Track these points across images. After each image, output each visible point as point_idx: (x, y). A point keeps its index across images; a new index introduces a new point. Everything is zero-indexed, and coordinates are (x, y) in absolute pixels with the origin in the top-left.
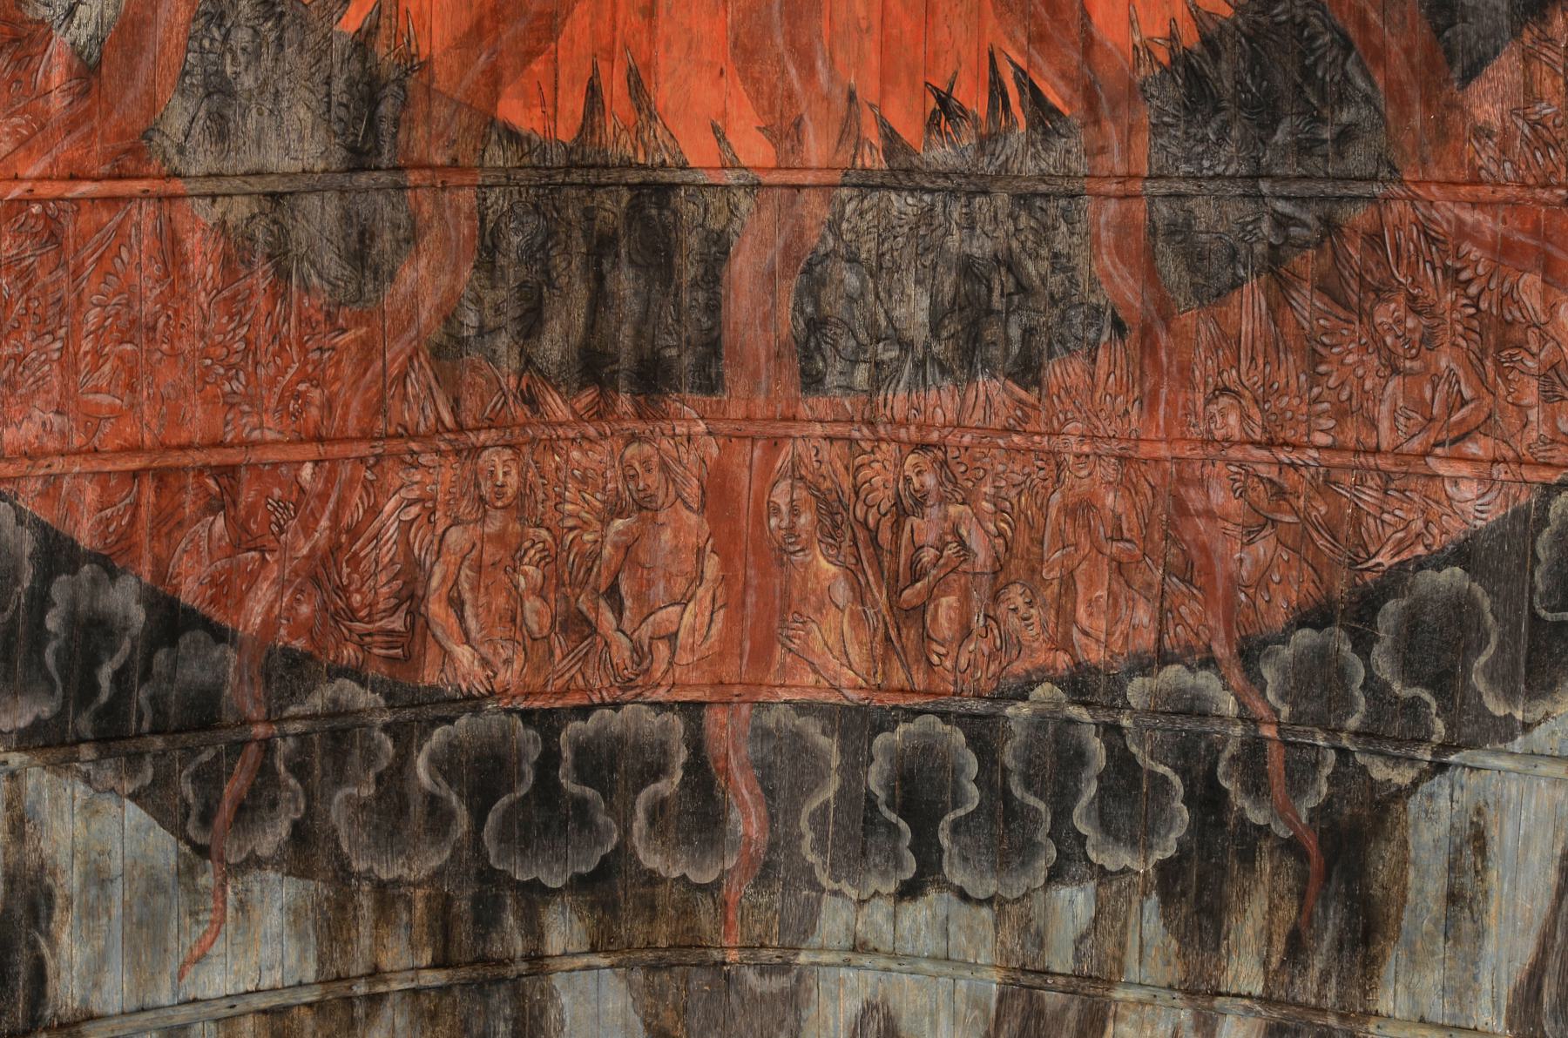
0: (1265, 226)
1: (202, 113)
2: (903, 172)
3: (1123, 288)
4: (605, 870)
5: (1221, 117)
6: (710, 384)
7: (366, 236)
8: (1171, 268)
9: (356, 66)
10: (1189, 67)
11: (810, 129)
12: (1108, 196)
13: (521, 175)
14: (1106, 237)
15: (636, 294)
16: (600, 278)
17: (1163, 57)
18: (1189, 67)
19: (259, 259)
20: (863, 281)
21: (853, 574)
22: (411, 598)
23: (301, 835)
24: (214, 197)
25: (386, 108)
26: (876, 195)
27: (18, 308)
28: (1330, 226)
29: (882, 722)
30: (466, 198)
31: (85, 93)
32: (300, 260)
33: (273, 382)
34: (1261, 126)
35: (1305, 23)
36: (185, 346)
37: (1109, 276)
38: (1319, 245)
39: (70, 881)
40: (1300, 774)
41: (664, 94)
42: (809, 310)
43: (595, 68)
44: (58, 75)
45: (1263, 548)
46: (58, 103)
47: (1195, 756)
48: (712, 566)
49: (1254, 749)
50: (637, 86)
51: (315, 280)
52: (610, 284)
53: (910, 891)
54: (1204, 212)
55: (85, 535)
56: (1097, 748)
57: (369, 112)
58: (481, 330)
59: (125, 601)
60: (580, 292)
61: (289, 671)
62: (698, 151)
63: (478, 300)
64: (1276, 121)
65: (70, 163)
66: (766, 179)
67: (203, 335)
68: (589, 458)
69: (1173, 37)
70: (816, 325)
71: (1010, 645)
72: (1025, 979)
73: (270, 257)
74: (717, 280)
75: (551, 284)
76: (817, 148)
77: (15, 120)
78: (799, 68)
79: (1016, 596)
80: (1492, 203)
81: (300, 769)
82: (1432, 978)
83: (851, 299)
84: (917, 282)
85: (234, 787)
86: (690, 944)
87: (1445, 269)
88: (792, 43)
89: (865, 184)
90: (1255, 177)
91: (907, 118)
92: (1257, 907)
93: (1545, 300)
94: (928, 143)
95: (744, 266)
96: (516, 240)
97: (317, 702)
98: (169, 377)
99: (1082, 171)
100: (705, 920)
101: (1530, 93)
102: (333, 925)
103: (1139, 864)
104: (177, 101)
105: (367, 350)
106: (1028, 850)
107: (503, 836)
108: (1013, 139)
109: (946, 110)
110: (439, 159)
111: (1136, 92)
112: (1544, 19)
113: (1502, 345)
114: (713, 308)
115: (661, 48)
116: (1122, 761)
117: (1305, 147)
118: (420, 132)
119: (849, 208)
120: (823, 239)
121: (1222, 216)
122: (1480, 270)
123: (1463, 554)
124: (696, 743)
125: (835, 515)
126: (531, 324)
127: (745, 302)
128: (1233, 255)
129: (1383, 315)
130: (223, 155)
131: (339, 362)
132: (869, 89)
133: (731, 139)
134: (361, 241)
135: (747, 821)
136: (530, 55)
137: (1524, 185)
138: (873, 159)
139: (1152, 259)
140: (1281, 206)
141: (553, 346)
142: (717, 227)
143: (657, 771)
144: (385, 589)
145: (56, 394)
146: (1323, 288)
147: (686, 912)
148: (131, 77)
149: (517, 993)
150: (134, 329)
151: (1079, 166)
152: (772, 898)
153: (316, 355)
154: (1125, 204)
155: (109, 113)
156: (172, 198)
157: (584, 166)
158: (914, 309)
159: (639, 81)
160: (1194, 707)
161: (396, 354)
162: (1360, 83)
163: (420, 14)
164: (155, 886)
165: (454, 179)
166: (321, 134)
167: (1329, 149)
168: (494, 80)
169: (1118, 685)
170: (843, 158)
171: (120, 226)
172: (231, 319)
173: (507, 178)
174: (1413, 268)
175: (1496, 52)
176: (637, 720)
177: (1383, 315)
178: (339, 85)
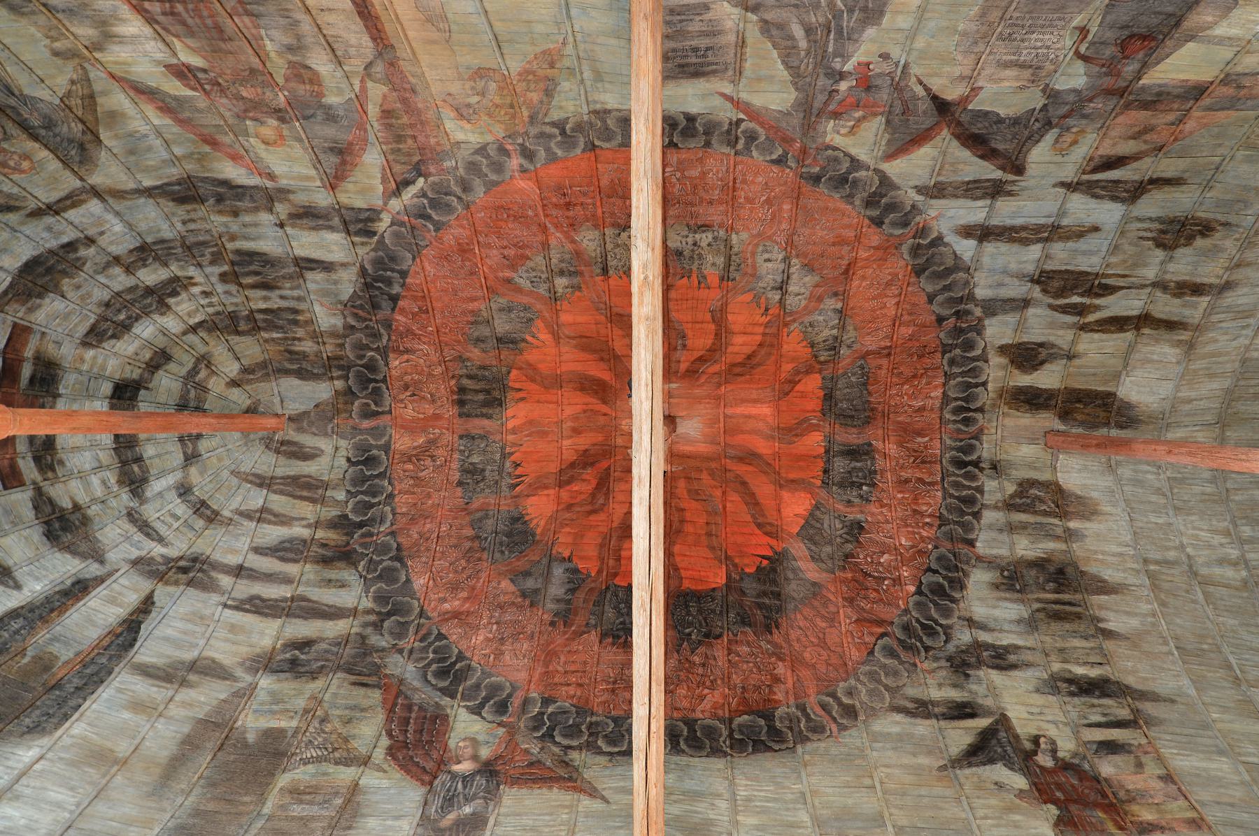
3: (475, 505)
4: (353, 393)
6: (460, 415)
7: (483, 341)
8: (479, 514)
21: (419, 447)
22: (407, 351)
23: (353, 327)
28: (484, 549)
29: (386, 453)
30: (494, 363)
39: (334, 276)
40: (364, 545)
41: (521, 405)
45: (416, 536)
46: (501, 274)
47: (372, 521)
48: (421, 416)
49: (371, 535)
50: (522, 399)
53: (349, 460)
54: (490, 522)
55: (408, 280)
56: (377, 500)
59: (396, 289)
60: (478, 387)
61: (388, 325)
62: (510, 412)
68: (443, 390)
70: (473, 438)
71: (401, 481)
72: (326, 486)
76: (510, 438)
79: (411, 482)
81: (367, 327)
82: (312, 577)
85: (361, 313)
86: (338, 412)
89: (503, 448)
92: (335, 536)
95: (486, 422)
97: (382, 331)
100: (344, 415)
102: (334, 334)
103: (348, 511)
105: (459, 342)
106: (355, 485)
107: (358, 371)
114: (477, 416)
116: (372, 506)
117: (501, 544)
123: (408, 581)
124: (383, 413)
125: (432, 442)
126: (469, 377)
129: (463, 562)
132: (522, 449)
135: (366, 424)
138: (508, 450)
141: (465, 382)
143: (376, 404)
144: (408, 346)
147: (346, 411)
149: (325, 374)
152: (349, 430)
157: (505, 389)
158: (475, 459)
160: (382, 522)
161: (459, 348)
164: (336, 295)
168: (520, 369)
169: (389, 504)
176: (387, 400)
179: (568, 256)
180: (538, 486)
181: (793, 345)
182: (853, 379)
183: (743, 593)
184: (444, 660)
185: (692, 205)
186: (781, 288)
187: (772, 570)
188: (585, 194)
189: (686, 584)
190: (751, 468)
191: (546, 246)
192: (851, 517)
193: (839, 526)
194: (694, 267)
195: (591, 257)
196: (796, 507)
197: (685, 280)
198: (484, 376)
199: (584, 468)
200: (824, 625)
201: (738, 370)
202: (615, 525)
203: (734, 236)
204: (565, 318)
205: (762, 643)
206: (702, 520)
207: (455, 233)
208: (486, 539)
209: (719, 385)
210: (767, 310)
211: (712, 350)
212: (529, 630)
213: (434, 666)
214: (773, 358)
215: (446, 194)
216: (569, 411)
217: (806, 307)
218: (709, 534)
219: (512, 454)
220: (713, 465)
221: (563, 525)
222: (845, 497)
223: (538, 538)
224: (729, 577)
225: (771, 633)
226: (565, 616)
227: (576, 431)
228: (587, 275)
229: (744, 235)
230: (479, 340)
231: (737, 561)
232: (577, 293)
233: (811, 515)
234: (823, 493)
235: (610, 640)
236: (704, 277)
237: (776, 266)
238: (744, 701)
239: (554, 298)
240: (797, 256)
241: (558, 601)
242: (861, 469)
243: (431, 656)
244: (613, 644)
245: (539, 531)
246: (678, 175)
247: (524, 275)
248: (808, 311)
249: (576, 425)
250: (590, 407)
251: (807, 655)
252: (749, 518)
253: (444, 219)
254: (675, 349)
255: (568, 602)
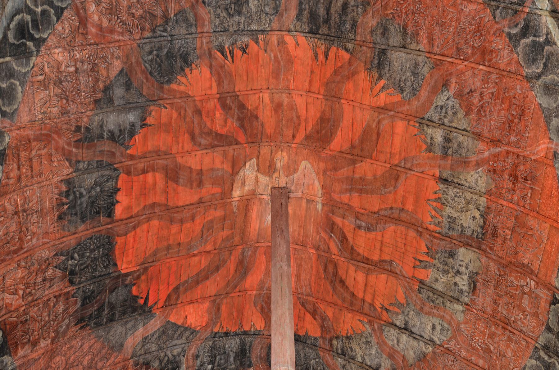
0: (169, 29)
1: (420, 69)
2: (254, 34)
5: (180, 53)
7: (383, 34)
8: (191, 17)
9: (382, 72)
10: (187, 63)
11: (276, 44)
12: (206, 32)
13: (345, 41)
14: (207, 23)
15: (319, 9)
16: (328, 14)
17: (193, 66)
18: (187, 63)
19: (410, 34)
20: (264, 9)
24: (419, 50)
25: (376, 62)
26: (261, 29)
27: (469, 36)
28: (154, 31)
30: (359, 38)
31: (447, 80)
32: (400, 32)
33: (409, 5)
34: (170, 52)
35: (160, 77)
36: (430, 18)
37: (206, 14)
38: (156, 26)
41: (310, 54)
42: (278, 2)
43: (326, 62)
44: (453, 86)
46: (454, 80)
50: (316, 56)
51: (397, 26)
52: (325, 12)
54: (184, 31)
57: (380, 61)
58: (357, 6)
60: (333, 11)
62: (302, 39)
63: (357, 14)
64: (167, 54)
65: (452, 66)
66: (287, 33)
67: (425, 19)
69: (191, 70)
73: (407, 34)
74: (299, 10)
75: (340, 15)
76: (274, 39)
77: (464, 79)
78: (278, 57)
80: (115, 42)
83: (267, 5)
84: (251, 9)
87: (126, 25)
88: (279, 63)
89: (263, 31)
90: (172, 40)
91: (253, 47)
93: (102, 21)
94: (248, 41)
95: (293, 12)
96: (347, 26)
98: (434, 11)
99: (212, 38)
101: (107, 69)
104: (425, 74)
108: (229, 44)
109: (244, 50)
110: (364, 48)
111: (199, 57)
112: (105, 87)
113: (112, 8)
115: (310, 64)
117: (160, 48)
118: (369, 55)
119: (267, 26)
120: (274, 18)
121: (179, 30)
122: (117, 26)
127: (293, 4)
128: (177, 21)
129: (141, 12)
130: (415, 59)
131: (393, 6)
132: (262, 53)
133: (294, 42)
134: (385, 33)
136: (341, 67)
137: (108, 47)
138: (261, 37)
139: (196, 19)
140: (165, 34)
142: (299, 22)
145: (462, 14)
146: (155, 16)
148: (436, 82)
150: (442, 24)
151: (213, 39)
153: (398, 9)
154: (202, 31)
155: (442, 75)
156: (429, 53)
157: (330, 39)
159: (316, 57)
162: (147, 65)
163: (366, 81)
165: (361, 43)
166: (392, 59)
167: (154, 49)
168: (350, 63)
170: (268, 37)
171: (442, 49)
172: (418, 22)
173: (349, 40)
174: (134, 24)
175: (116, 77)
177: (141, 12)
178: (387, 69)
179: (464, 153)
180: (220, 75)
181: (349, 322)
182: (313, 362)
183: (112, 291)
184: (36, 25)
185: (496, 287)
186: (406, 329)
187: (136, 308)
188: (523, 197)
189: (120, 241)
190: (232, 271)
191: (478, 136)
192: (184, 360)
193: (175, 352)
194: (436, 262)
195: (460, 173)
196: (194, 315)
197: (424, 249)
198: (345, 22)
199: (239, 119)
200: (85, 363)
201: (331, 269)
202: (179, 160)
203: (461, 308)
204: (400, 126)
205: (67, 321)
206: (182, 239)
207: (505, 56)
208: (165, 30)
209: (317, 249)
210: (387, 310)
211: (352, 251)
212: (72, 107)
213: (28, 18)
214: (339, 302)
215: (545, 65)
216: (300, 102)
217: (386, 344)
218: (168, 248)
219: (257, 42)
220: (237, 239)
221: (179, 109)
222: (201, 352)
223: (166, 87)
224: (127, 275)
225: (76, 325)
226: (86, 137)
227: (278, 107)
228: (442, 162)
229: (460, 317)
230: (385, 31)
231: (143, 277)
232: (424, 147)
233: (186, 329)
234: (207, 334)
235: (64, 189)
236: (425, 267)
237: (428, 332)
238: (14, 326)
239: (423, 122)
240: (434, 353)
241: (101, 127)
242: (227, 361)
243: (39, 10)
244: (60, 194)
245: (173, 86)
246: (527, 289)
247: (450, 103)
248: (382, 344)
249: (285, 107)
250: (303, 124)
251: (58, 358)
252: (184, 278)
253: (520, 48)
254: (357, 218)
255: (101, 137)
